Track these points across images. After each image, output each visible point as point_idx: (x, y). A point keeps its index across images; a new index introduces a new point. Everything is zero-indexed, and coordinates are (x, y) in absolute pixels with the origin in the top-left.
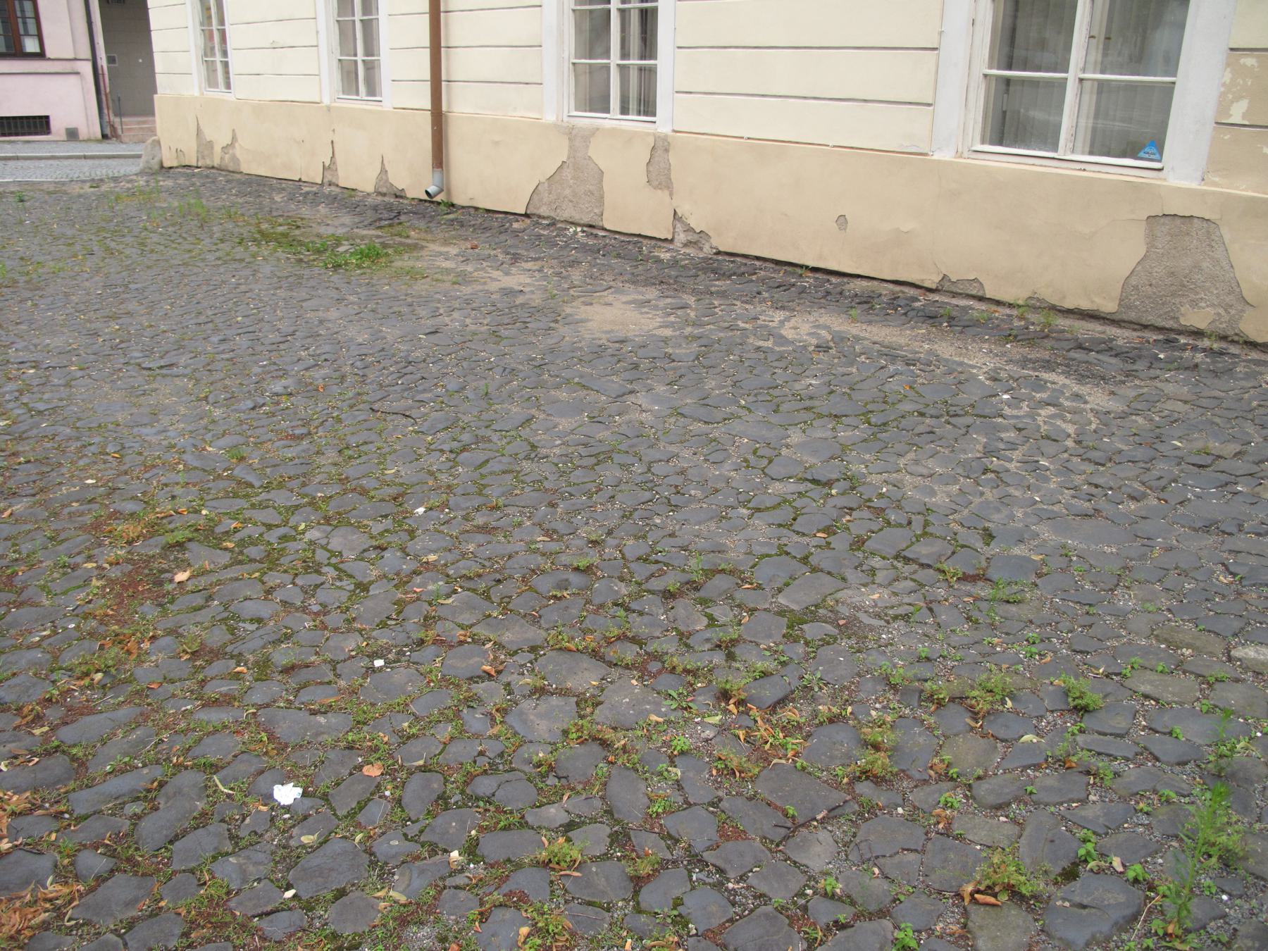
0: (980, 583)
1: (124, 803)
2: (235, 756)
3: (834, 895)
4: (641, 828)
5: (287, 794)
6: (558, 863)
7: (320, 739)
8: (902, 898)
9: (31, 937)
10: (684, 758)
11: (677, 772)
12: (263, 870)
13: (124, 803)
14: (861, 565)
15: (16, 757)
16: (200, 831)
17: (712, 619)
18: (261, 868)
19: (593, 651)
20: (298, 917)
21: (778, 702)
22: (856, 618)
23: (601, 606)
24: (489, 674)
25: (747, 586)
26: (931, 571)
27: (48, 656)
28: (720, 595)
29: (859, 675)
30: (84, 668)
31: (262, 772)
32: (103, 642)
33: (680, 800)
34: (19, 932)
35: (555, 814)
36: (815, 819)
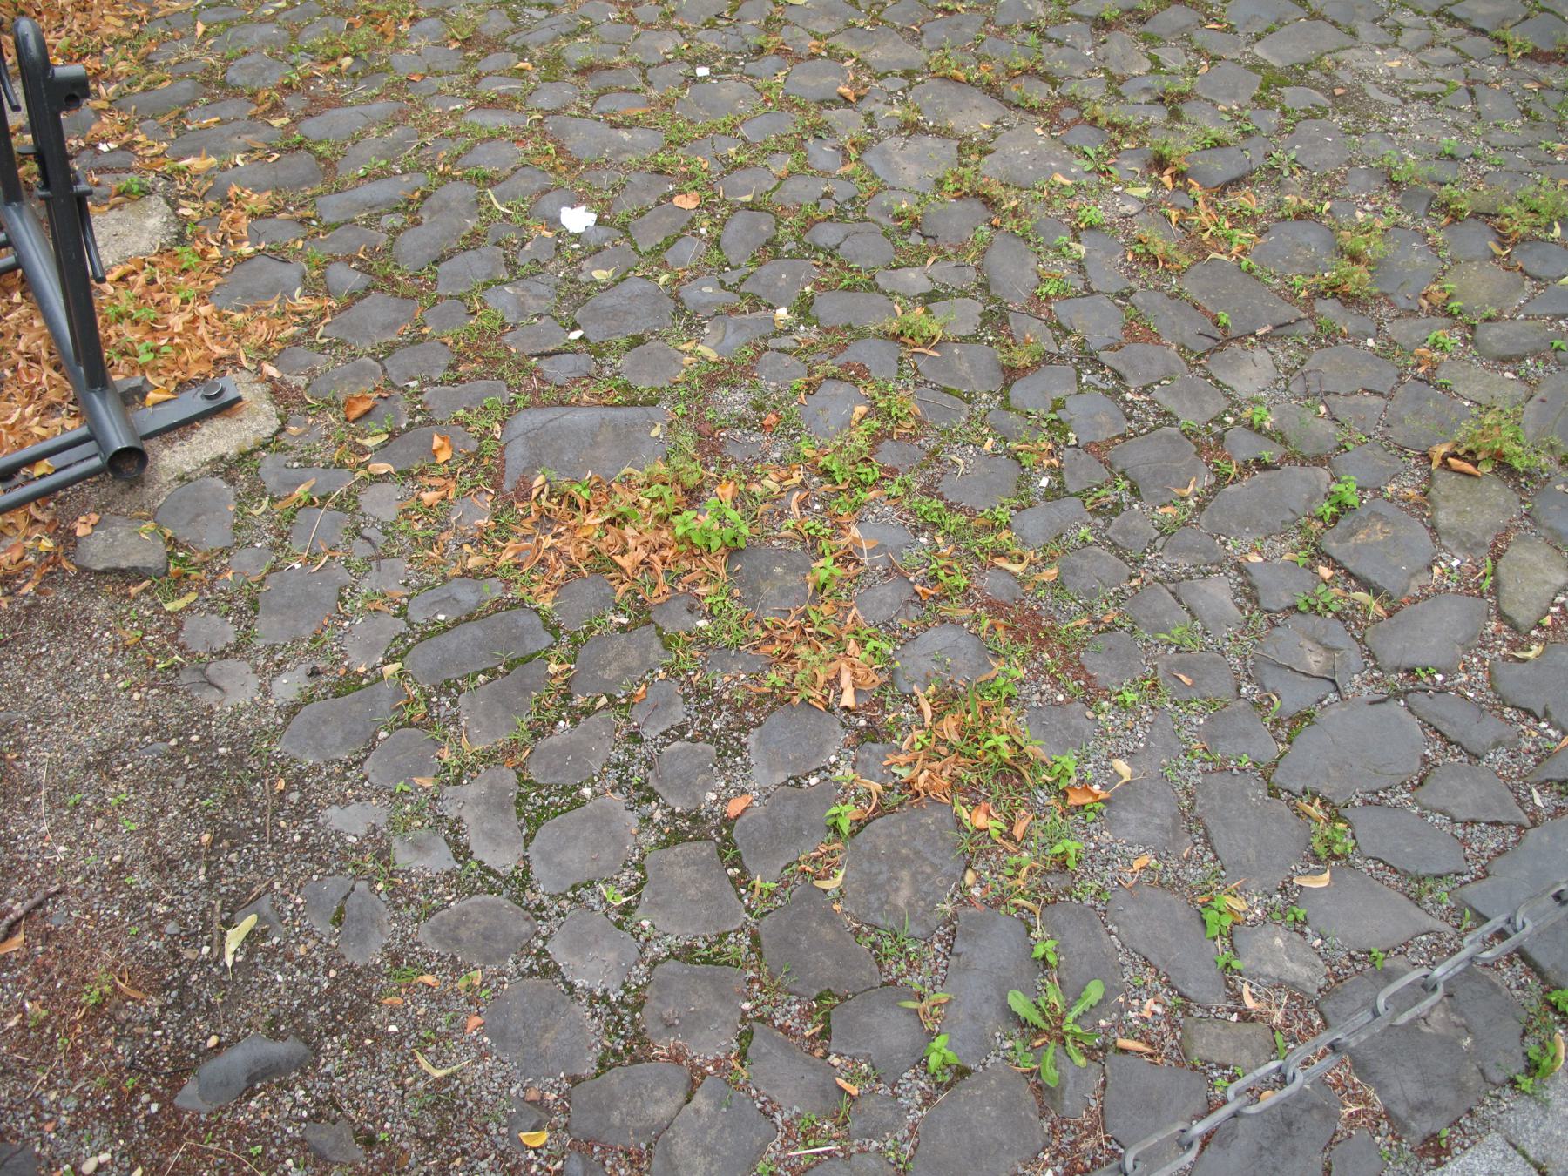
0: (1555, 66)
1: (381, 214)
2: (515, 170)
3: (1261, 429)
4: (1022, 311)
5: (577, 219)
6: (911, 338)
7: (621, 158)
8: (1350, 446)
9: (280, 351)
10: (1092, 233)
11: (1080, 250)
12: (545, 305)
13: (381, 214)
14: (1382, 18)
15: (253, 151)
16: (471, 253)
17: (1157, 63)
18: (543, 302)
19: (989, 84)
20: (584, 362)
21: (1230, 183)
22: (1361, 90)
23: (1007, 28)
24: (846, 99)
25: (1213, 26)
26: (1485, 40)
27: (285, 33)
28: (1173, 33)
29: (1349, 163)
30: (329, 51)
31: (548, 191)
32: (351, 20)
33: (1080, 285)
34: (267, 343)
35: (915, 279)
36: (1253, 334)
